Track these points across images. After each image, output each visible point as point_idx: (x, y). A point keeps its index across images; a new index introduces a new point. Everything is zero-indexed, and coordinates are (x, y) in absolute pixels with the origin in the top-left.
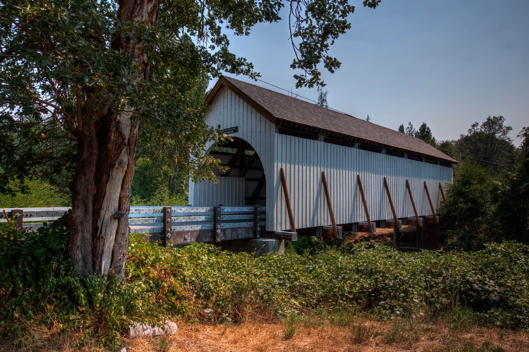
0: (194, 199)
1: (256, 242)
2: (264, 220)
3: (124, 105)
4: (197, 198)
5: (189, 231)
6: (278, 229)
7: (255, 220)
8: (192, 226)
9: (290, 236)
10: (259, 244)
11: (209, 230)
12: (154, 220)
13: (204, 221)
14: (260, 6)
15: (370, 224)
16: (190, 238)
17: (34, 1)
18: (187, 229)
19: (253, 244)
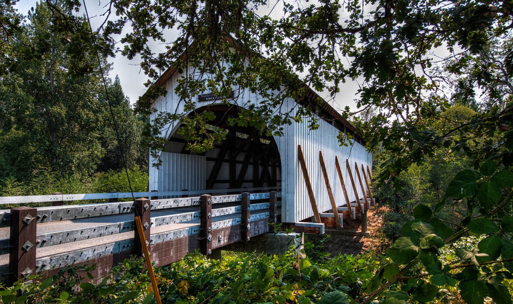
0: (158, 182)
1: (275, 237)
2: (279, 207)
3: (201, 99)
4: (162, 182)
5: (222, 229)
6: (298, 220)
7: (271, 210)
8: (224, 221)
9: (319, 228)
10: (279, 239)
11: (236, 226)
12: (191, 215)
13: (234, 213)
14: (285, 51)
15: (350, 209)
16: (223, 238)
17: (511, 11)
18: (220, 227)
19: (269, 240)
